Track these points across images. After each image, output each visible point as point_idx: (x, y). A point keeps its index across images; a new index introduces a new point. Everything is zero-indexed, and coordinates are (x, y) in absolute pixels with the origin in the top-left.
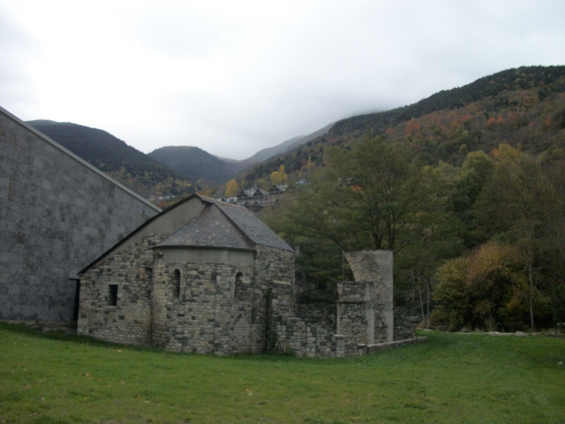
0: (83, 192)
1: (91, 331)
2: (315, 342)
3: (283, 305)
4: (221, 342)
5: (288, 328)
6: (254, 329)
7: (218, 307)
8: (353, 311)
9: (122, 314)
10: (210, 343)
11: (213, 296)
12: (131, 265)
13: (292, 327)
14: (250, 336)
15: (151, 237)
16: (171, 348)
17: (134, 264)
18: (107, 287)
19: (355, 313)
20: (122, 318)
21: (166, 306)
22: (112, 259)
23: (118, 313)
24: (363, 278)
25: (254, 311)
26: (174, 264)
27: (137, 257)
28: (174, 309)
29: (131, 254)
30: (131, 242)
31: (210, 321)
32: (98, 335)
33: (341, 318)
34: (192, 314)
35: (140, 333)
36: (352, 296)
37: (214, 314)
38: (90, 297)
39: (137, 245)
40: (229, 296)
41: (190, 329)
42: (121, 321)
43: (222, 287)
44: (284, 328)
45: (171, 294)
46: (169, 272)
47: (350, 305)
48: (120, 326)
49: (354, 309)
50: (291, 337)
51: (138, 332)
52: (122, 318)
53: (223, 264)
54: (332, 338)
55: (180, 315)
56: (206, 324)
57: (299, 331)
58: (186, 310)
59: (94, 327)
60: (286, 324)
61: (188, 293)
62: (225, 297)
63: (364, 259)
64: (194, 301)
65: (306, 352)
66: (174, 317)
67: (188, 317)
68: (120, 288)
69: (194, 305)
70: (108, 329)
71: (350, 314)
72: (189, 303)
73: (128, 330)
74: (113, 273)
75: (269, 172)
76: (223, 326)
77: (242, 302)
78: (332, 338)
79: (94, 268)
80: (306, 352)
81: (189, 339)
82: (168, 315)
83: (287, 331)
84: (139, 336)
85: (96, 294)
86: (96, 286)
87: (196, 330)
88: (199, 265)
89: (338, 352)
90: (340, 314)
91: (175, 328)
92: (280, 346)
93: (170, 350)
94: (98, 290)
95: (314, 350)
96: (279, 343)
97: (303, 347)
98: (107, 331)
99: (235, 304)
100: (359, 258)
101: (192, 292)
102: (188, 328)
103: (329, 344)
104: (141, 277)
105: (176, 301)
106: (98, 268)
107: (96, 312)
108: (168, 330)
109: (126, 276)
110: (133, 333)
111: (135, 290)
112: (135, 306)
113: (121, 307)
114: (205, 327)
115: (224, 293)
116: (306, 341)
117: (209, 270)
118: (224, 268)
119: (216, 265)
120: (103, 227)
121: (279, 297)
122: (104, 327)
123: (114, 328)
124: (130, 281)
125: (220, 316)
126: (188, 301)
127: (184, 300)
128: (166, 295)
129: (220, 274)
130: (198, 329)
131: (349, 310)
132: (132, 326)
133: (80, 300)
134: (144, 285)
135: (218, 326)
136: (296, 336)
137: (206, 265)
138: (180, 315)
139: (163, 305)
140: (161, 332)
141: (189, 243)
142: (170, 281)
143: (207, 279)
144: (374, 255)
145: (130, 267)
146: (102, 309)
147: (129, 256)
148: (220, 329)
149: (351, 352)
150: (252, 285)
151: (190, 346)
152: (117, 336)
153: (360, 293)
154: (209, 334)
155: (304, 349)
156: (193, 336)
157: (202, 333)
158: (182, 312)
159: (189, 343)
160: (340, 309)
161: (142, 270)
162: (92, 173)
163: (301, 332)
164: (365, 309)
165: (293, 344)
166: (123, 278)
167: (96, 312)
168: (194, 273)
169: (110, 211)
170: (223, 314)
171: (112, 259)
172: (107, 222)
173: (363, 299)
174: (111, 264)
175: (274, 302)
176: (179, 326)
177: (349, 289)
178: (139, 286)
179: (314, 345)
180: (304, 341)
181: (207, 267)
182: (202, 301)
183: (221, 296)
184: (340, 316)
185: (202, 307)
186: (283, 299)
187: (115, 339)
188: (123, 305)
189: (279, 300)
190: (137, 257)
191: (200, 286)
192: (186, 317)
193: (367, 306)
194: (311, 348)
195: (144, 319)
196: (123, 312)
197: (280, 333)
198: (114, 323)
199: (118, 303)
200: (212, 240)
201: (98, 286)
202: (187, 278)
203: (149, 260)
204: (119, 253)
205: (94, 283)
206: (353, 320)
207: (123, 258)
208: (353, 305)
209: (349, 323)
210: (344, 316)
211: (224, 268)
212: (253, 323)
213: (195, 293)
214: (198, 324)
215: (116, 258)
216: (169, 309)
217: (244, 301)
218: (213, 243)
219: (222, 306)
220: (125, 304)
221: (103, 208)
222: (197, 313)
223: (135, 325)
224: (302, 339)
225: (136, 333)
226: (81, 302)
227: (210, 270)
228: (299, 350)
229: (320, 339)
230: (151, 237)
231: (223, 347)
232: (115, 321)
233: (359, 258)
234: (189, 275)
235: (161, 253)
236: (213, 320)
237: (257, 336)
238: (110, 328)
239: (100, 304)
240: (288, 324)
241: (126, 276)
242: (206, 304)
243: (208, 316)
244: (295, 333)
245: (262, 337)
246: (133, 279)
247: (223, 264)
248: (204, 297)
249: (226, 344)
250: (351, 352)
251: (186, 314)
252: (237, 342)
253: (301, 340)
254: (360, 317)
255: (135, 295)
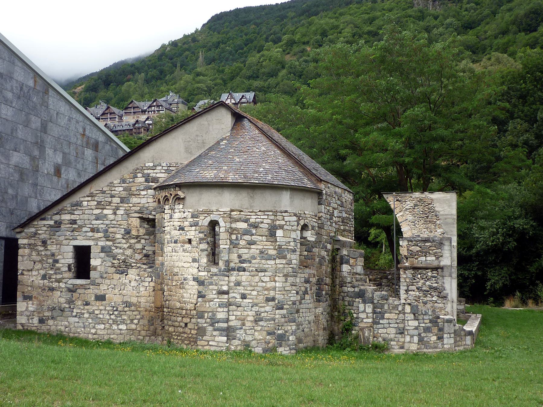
0: (10, 95)
1: (41, 321)
2: (416, 328)
3: (357, 274)
4: (286, 332)
5: (374, 308)
6: (319, 310)
7: (280, 279)
8: (425, 281)
9: (99, 293)
10: (269, 334)
11: (273, 262)
12: (115, 214)
13: (382, 306)
14: (317, 321)
15: (149, 168)
16: (208, 345)
17: (121, 212)
18: (71, 249)
19: (428, 283)
20: (101, 298)
21: (195, 279)
22: (78, 204)
23: (92, 291)
24: (415, 232)
25: (319, 282)
26: (209, 212)
27: (123, 200)
28: (211, 284)
29: (112, 196)
30: (114, 177)
31: (268, 300)
32: (53, 326)
33: (407, 291)
34: (241, 289)
35: (136, 321)
36: (423, 259)
37: (274, 289)
38: (38, 266)
39: (123, 181)
40: (294, 262)
41: (239, 313)
42: (98, 303)
43: (285, 247)
44: (369, 309)
45: (204, 260)
46: (200, 224)
47: (420, 271)
48: (97, 312)
49: (426, 277)
50: (381, 322)
51: (132, 320)
52: (101, 298)
53: (286, 212)
54: (439, 321)
55: (221, 293)
56: (263, 305)
57: (392, 311)
58: (232, 284)
59: (47, 314)
60: (372, 303)
61: (234, 257)
62: (289, 263)
63: (416, 205)
64: (244, 270)
65: (404, 342)
66: (211, 296)
67: (235, 295)
68: (94, 251)
69: (244, 277)
70: (76, 316)
71: (420, 284)
72: (235, 273)
73: (113, 317)
74: (81, 227)
75: (120, 83)
76: (288, 307)
77: (307, 270)
78: (439, 321)
79: (44, 219)
80: (404, 342)
81: (237, 329)
82: (199, 292)
83: (374, 312)
84: (134, 326)
85: (51, 261)
86: (49, 247)
87: (248, 315)
88: (250, 214)
89: (445, 341)
90: (405, 284)
91: (214, 313)
92: (364, 335)
93: (207, 348)
94: (53, 255)
95: (416, 339)
96: (362, 329)
97: (400, 336)
98: (72, 320)
99: (301, 273)
100: (409, 204)
101: (239, 256)
102: (235, 313)
103: (435, 330)
104: (134, 233)
105: (214, 270)
106: (51, 219)
107: (52, 289)
108: (201, 315)
109: (106, 231)
110: (123, 322)
111: (123, 254)
112: (124, 279)
113: (99, 281)
114: (262, 310)
115: (288, 256)
116: (405, 326)
117: (265, 221)
118: (286, 219)
119: (275, 213)
120: (36, 153)
121: (352, 261)
122: (67, 313)
123: (86, 315)
124: (113, 240)
125: (284, 293)
126: (233, 269)
127: (229, 270)
128: (194, 260)
129: (281, 227)
130: (250, 313)
131: (418, 278)
132: (120, 311)
133: (20, 272)
134: (139, 246)
135: (282, 308)
136: (389, 319)
137: (259, 213)
138: (221, 293)
139: (190, 277)
140: (186, 320)
141: (231, 178)
142: (201, 239)
143: (262, 236)
144: (432, 199)
145: (112, 217)
146: (62, 285)
147: (110, 199)
148: (284, 312)
149: (459, 341)
150: (317, 243)
151: (239, 340)
152: (94, 327)
153: (435, 255)
154: (267, 320)
155: (402, 337)
156: (244, 324)
157: (257, 320)
158: (225, 288)
159: (238, 335)
160: (405, 276)
161: (135, 222)
162: (20, 64)
163: (396, 314)
164: (443, 277)
165: (384, 331)
166: (100, 235)
167: (52, 289)
168: (243, 225)
169: (44, 128)
170: (286, 288)
171: (78, 204)
172: (41, 146)
173: (440, 262)
174: (76, 212)
175: (345, 268)
176: (219, 309)
177: (418, 249)
178: (130, 247)
179: (416, 332)
180: (401, 326)
181: (262, 217)
182: (256, 270)
183: (284, 261)
184: (406, 288)
185: (257, 279)
186: (356, 265)
187: (89, 333)
188: (102, 277)
189: (350, 266)
190: (123, 200)
191: (252, 247)
192: (231, 295)
193: (446, 272)
194: (412, 336)
195: (143, 300)
196: (103, 289)
197: (362, 315)
198: (86, 307)
199: (92, 274)
200: (266, 173)
201: (53, 248)
202: (231, 234)
203: (147, 205)
204: (91, 195)
205: (44, 243)
206: (426, 293)
207: (99, 203)
208: (424, 272)
209: (419, 297)
210: (411, 288)
211: (286, 219)
212: (319, 301)
213: (245, 257)
214: (250, 305)
215: (85, 204)
216: (200, 282)
217: (310, 268)
218: (269, 179)
219: (286, 276)
220: (105, 276)
221: (36, 122)
222: (249, 288)
223: (126, 309)
224: (398, 323)
225: (129, 322)
226: (22, 274)
227: (266, 221)
228: (394, 341)
229: (424, 323)
230: (149, 168)
231: (288, 340)
232: (87, 304)
233: (409, 204)
234: (236, 229)
235: (181, 194)
236: (273, 299)
237: (323, 321)
238: (79, 316)
239: (59, 276)
240: (375, 302)
241: (106, 231)
242: (263, 274)
243: (266, 292)
244: (387, 315)
245: (327, 321)
246: (118, 236)
247: (286, 212)
248: (259, 263)
249: (292, 334)
250: (459, 341)
251: (231, 291)
252: (303, 331)
253: (396, 325)
254: (435, 289)
255: (124, 261)
